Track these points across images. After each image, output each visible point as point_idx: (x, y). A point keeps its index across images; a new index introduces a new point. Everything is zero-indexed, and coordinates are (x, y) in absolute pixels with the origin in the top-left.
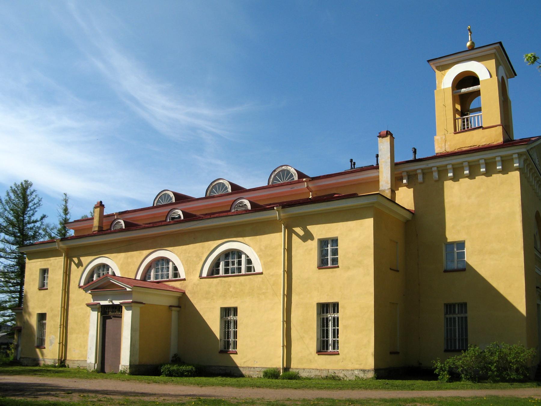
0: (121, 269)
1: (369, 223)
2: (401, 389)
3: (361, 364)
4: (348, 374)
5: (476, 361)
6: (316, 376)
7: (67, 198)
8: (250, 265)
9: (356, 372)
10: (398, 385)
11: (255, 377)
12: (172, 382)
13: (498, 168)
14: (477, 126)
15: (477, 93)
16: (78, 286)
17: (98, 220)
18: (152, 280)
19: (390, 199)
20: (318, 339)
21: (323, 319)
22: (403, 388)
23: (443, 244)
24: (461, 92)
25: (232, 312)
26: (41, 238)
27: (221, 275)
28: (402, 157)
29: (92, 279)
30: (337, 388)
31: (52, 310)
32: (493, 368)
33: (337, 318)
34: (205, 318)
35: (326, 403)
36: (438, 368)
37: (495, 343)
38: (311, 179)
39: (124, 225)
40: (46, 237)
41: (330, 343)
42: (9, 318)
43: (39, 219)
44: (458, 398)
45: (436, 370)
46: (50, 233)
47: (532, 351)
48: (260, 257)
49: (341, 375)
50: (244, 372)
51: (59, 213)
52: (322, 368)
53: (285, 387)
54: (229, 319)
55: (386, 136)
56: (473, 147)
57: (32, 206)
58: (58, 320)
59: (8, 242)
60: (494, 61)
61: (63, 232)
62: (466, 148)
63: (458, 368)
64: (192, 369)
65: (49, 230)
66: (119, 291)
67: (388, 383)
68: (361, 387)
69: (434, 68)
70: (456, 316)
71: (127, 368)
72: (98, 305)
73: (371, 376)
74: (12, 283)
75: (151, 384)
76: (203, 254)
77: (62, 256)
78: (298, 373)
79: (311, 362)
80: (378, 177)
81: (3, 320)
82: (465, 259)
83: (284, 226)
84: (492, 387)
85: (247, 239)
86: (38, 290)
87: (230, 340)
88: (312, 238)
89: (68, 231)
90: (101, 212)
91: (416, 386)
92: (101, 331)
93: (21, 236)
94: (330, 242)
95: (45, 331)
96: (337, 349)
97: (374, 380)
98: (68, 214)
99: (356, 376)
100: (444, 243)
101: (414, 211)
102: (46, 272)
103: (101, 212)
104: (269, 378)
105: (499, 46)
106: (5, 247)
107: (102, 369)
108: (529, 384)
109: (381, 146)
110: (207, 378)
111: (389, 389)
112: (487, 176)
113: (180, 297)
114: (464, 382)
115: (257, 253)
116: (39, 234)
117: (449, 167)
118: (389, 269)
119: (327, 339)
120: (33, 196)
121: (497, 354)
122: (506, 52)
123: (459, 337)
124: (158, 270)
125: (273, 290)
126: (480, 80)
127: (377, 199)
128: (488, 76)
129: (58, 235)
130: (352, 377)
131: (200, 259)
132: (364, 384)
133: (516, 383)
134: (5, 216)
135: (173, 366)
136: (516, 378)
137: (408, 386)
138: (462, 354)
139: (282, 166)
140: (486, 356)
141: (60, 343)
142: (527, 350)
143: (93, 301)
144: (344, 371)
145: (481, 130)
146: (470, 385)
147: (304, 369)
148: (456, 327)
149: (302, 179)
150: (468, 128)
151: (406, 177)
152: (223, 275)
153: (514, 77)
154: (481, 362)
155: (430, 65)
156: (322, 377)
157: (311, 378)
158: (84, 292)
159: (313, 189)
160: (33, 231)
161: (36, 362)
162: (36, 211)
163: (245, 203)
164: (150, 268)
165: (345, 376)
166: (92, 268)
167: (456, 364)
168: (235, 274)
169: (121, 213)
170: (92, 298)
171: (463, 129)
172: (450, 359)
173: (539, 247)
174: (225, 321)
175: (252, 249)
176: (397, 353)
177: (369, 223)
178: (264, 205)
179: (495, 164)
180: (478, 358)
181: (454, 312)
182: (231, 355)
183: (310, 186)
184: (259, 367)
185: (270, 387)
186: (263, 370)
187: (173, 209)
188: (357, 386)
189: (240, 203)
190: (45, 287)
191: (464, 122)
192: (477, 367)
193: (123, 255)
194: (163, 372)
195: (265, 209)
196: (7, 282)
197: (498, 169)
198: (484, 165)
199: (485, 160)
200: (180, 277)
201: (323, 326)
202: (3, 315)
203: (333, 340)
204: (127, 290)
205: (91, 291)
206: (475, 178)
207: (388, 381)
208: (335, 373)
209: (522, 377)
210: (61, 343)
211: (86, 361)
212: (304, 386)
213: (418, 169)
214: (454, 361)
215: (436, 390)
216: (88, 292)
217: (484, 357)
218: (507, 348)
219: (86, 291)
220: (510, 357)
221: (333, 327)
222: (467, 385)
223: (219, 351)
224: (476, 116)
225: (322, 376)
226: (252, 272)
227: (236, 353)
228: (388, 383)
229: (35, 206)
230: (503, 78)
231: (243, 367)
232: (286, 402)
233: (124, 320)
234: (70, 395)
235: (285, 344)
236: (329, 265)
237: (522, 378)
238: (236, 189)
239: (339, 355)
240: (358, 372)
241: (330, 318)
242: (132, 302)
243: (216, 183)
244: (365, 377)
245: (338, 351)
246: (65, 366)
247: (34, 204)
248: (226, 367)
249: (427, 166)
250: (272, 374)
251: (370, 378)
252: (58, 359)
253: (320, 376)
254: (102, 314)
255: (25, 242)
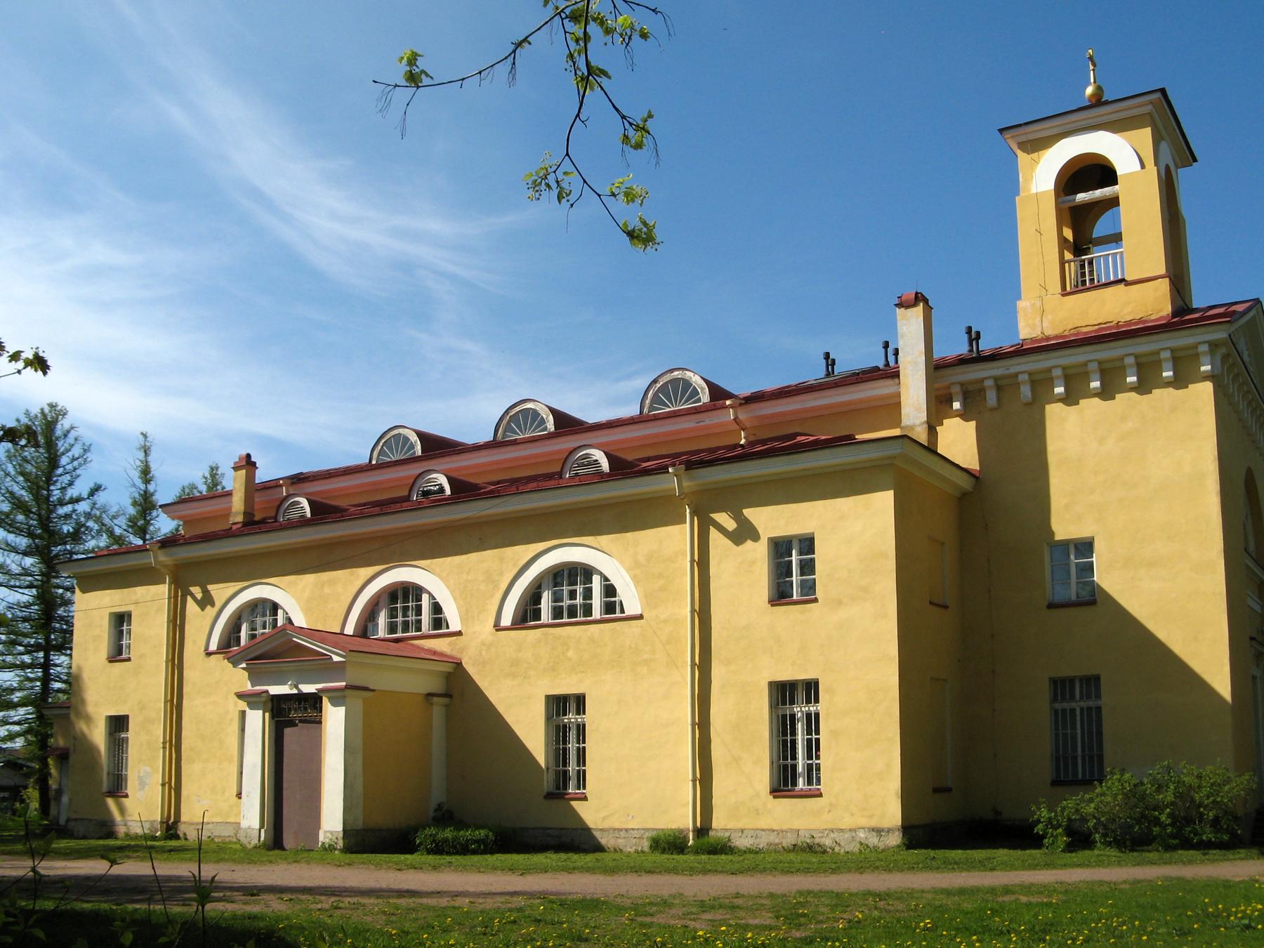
0: (307, 611)
1: (884, 501)
2: (965, 869)
3: (871, 817)
4: (843, 838)
5: (1126, 804)
6: (769, 844)
7: (148, 444)
8: (613, 599)
9: (862, 835)
10: (957, 860)
11: (630, 850)
12: (450, 867)
13: (1165, 374)
14: (1112, 279)
15: (1114, 202)
16: (205, 651)
17: (243, 498)
18: (382, 637)
19: (926, 445)
20: (772, 763)
21: (784, 717)
22: (970, 866)
23: (1045, 545)
24: (1077, 201)
25: (573, 706)
26: (90, 537)
27: (546, 622)
28: (953, 346)
29: (238, 635)
30: (825, 871)
31: (142, 708)
32: (1163, 818)
33: (815, 714)
34: (510, 719)
35: (823, 899)
36: (1043, 822)
37: (1166, 763)
38: (743, 402)
39: (308, 510)
40: (102, 535)
41: (800, 770)
42: (19, 726)
43: (85, 495)
44: (1101, 883)
45: (1036, 826)
46: (110, 527)
47: (1248, 781)
48: (636, 579)
49: (827, 842)
50: (603, 841)
51: (129, 479)
52: (785, 827)
53: (709, 871)
54: (566, 721)
55: (915, 304)
56: (1104, 326)
57: (68, 464)
58: (158, 732)
59: (14, 549)
60: (1149, 130)
61: (141, 523)
62: (1088, 327)
63: (1088, 821)
64: (487, 836)
65: (107, 521)
66: (315, 663)
67: (934, 857)
68: (877, 868)
69: (1015, 147)
70: (1078, 705)
71: (337, 838)
72: (263, 695)
73: (895, 843)
74: (25, 646)
75: (405, 871)
76: (501, 574)
77: (165, 583)
78: (729, 840)
79: (758, 813)
80: (898, 395)
81: (6, 733)
82: (1095, 579)
83: (690, 510)
84: (1164, 861)
85: (604, 540)
86: (106, 662)
87: (570, 769)
88: (755, 537)
89: (152, 522)
90: (250, 478)
91: (997, 862)
92: (273, 753)
93: (46, 536)
94: (795, 544)
95: (127, 757)
96: (816, 785)
97: (903, 850)
98: (151, 482)
99: (861, 844)
100: (1047, 544)
101: (979, 471)
102: (126, 619)
103: (250, 478)
104: (664, 851)
105: (1159, 98)
106: (5, 560)
107: (276, 842)
108: (1243, 853)
109: (904, 328)
110: (527, 856)
111: (940, 870)
112: (1141, 393)
113: (450, 673)
114: (1100, 851)
115: (628, 570)
116: (87, 530)
117: (1057, 373)
118: (928, 602)
119: (793, 762)
120: (70, 439)
121: (1172, 787)
122: (1175, 110)
123: (1083, 751)
124: (395, 613)
125: (669, 655)
126: (1118, 174)
127: (902, 448)
128: (1136, 166)
129: (128, 532)
130: (853, 844)
131: (496, 587)
132: (882, 860)
133: (1214, 852)
134: (7, 488)
135: (443, 830)
136: (1213, 839)
137: (980, 861)
138: (1096, 788)
139: (672, 371)
140: (1147, 792)
141: (163, 785)
142: (1236, 777)
143: (252, 687)
144: (833, 832)
145: (1122, 286)
146: (1115, 856)
147: (742, 831)
148: (1076, 729)
149: (721, 402)
150: (1092, 280)
151: (960, 397)
152: (550, 621)
153: (1191, 165)
154: (1136, 806)
155: (1005, 139)
156: (783, 847)
157: (758, 849)
158: (231, 665)
159: (748, 425)
160: (71, 523)
161: (106, 828)
162: (78, 476)
163: (595, 458)
164: (376, 608)
165: (836, 843)
166: (238, 608)
167: (1083, 812)
168: (563, 620)
169: (298, 480)
170: (249, 679)
171: (1082, 285)
172: (1069, 802)
173: (1252, 547)
174: (558, 727)
175: (615, 561)
176: (949, 790)
177: (884, 501)
178: (635, 460)
179: (1157, 365)
180: (1129, 798)
181: (1072, 698)
182: (573, 803)
183: (742, 416)
184: (638, 829)
185: (669, 871)
186: (647, 834)
187: (424, 472)
188: (868, 865)
189: (584, 457)
190: (124, 656)
191: (1083, 267)
192: (1128, 817)
193: (309, 579)
194: (421, 844)
195: (647, 472)
196: (14, 643)
197: (1167, 377)
198: (1134, 369)
199: (1136, 357)
200: (448, 627)
201: (785, 734)
202: (5, 722)
203: (808, 764)
204: (334, 660)
205: (247, 664)
206: (1114, 398)
207: (934, 851)
208: (813, 837)
209: (1226, 837)
210: (167, 785)
211: (239, 823)
212: (751, 868)
213: (986, 378)
214: (1078, 805)
215: (1043, 869)
216: (240, 666)
217: (1143, 797)
218: (1193, 774)
219: (235, 664)
220: (1201, 795)
221: (807, 735)
222: (1109, 856)
223: (545, 794)
224: (1109, 254)
225: (784, 845)
226: (618, 615)
227: (585, 799)
228: (936, 856)
229: (76, 463)
230: (1167, 168)
231: (601, 829)
232: (736, 900)
233: (328, 727)
234: (256, 897)
235: (698, 776)
236: (795, 597)
237: (1226, 838)
238: (566, 423)
239: (822, 796)
240: (867, 834)
241: (799, 714)
242: (347, 687)
243: (518, 409)
244: (881, 846)
245: (819, 789)
246: (177, 837)
247: (74, 459)
248: (562, 829)
249: (1007, 372)
250: (670, 844)
251: (893, 848)
252: (159, 820)
253: (780, 846)
254: (273, 717)
255: (53, 548)
